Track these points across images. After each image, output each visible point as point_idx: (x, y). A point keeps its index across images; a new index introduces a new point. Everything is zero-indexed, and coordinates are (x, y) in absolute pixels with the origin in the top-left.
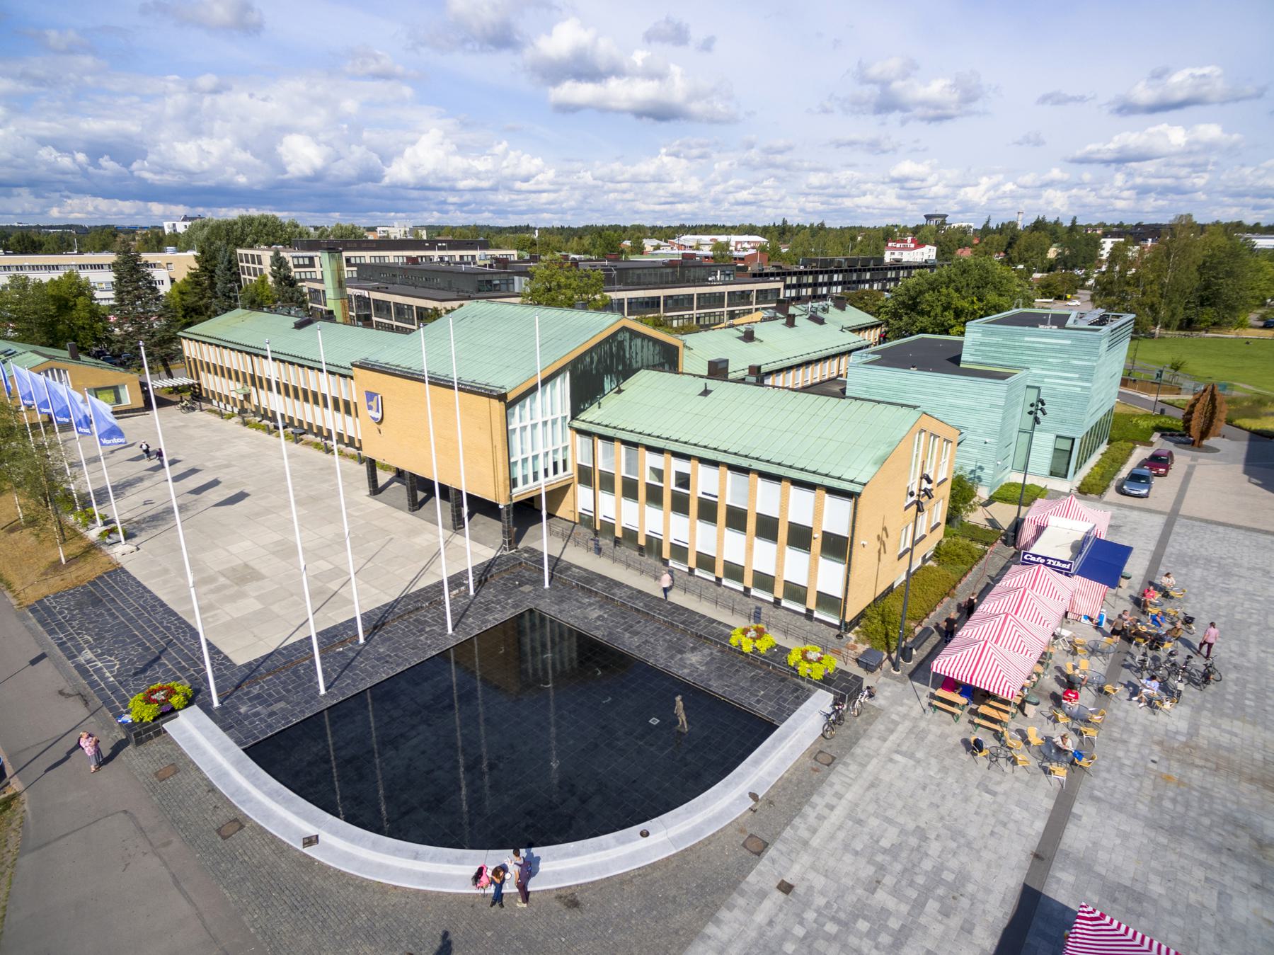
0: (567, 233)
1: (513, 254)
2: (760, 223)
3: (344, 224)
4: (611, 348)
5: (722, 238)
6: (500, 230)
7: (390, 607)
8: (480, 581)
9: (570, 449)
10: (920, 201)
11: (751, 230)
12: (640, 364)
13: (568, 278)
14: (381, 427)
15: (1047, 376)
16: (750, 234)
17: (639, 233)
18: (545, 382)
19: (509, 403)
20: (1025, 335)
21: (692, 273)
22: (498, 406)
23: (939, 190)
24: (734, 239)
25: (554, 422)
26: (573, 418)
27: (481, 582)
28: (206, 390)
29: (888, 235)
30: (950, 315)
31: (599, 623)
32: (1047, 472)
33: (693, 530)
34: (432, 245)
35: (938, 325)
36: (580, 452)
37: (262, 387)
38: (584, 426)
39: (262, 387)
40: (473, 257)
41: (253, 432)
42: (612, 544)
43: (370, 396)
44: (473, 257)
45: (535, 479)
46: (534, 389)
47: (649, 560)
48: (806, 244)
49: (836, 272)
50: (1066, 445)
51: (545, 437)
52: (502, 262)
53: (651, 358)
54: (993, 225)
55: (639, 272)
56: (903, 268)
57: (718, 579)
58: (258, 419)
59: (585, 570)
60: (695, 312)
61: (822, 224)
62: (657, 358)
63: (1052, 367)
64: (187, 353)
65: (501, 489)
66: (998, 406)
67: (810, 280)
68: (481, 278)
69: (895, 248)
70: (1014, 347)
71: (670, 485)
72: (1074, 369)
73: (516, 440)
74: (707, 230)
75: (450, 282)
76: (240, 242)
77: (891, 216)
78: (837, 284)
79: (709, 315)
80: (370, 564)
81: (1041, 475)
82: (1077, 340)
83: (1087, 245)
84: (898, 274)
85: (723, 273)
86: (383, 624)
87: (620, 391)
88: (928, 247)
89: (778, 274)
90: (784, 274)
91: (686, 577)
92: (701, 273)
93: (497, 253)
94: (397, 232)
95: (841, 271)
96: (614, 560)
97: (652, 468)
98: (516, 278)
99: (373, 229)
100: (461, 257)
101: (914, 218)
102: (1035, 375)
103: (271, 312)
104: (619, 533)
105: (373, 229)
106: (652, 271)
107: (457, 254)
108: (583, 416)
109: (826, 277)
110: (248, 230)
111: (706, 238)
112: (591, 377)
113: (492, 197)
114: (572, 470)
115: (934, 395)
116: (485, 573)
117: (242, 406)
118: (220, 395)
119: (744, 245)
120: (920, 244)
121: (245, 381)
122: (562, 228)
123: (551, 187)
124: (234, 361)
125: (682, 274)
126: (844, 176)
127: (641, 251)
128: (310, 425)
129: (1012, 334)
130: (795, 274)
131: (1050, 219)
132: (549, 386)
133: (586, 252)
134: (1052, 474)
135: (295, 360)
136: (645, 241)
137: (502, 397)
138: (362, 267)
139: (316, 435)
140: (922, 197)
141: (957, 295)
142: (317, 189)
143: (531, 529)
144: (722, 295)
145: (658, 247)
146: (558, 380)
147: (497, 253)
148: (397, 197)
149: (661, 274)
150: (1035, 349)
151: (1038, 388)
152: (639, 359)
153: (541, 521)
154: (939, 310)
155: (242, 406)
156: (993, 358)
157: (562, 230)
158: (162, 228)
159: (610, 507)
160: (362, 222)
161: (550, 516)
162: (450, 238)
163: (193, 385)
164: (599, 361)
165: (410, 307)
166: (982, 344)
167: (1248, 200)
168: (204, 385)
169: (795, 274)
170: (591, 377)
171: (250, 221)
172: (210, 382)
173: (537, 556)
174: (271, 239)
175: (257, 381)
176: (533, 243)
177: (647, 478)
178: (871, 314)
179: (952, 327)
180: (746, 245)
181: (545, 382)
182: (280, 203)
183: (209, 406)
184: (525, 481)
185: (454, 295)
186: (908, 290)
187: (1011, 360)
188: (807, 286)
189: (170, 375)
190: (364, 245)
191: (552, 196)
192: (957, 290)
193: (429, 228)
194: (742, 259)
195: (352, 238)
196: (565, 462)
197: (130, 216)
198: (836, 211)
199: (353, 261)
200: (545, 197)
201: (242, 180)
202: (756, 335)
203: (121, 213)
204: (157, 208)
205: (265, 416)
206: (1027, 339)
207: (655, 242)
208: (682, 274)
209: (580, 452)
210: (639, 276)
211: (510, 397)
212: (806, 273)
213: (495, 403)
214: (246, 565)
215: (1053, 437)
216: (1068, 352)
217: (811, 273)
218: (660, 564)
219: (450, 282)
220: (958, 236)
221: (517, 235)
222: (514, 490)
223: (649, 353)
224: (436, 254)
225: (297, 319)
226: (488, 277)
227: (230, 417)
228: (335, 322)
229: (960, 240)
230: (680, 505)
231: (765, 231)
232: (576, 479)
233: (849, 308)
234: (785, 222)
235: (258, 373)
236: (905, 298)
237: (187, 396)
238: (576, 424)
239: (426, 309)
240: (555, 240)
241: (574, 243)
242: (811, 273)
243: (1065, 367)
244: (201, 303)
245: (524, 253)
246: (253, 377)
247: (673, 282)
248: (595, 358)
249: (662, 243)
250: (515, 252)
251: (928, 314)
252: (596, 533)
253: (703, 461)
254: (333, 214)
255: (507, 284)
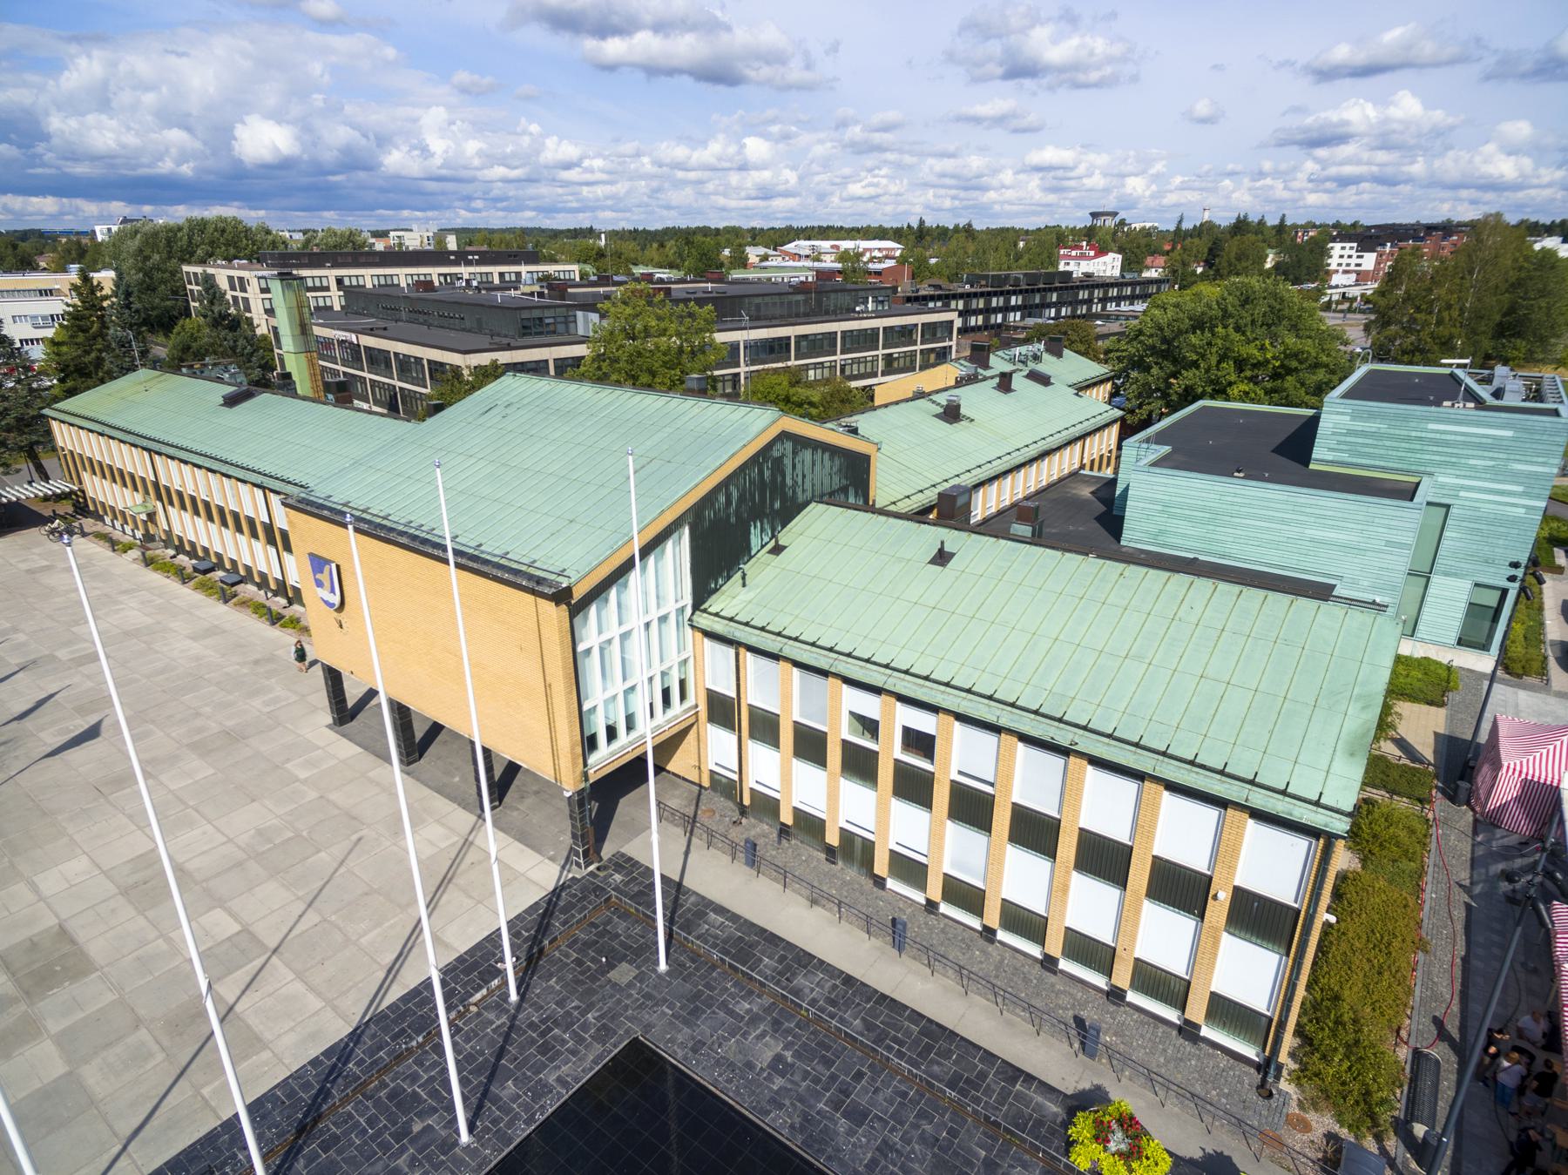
0: (642, 238)
1: (573, 270)
2: (889, 224)
3: (337, 227)
4: (761, 473)
5: (846, 245)
6: (555, 234)
7: (341, 1053)
8: (530, 959)
9: (691, 661)
10: (1073, 195)
11: (881, 233)
12: (809, 494)
13: (659, 318)
14: (343, 616)
15: (1463, 488)
16: (882, 238)
17: (739, 238)
18: (646, 551)
19: (574, 604)
20: (1429, 420)
21: (832, 301)
22: (554, 614)
23: (1096, 181)
24: (864, 244)
25: (663, 619)
26: (698, 605)
27: (530, 965)
28: (94, 501)
29: (1058, 238)
30: (1228, 366)
31: (778, 1082)
32: (1453, 639)
33: (936, 837)
34: (461, 258)
35: (1212, 382)
36: (715, 670)
37: (171, 503)
38: (719, 627)
39: (171, 503)
40: (518, 274)
41: (155, 578)
42: (775, 835)
43: (318, 563)
44: (518, 274)
45: (630, 727)
46: (628, 565)
47: (849, 873)
48: (960, 252)
49: (1014, 293)
50: (1491, 599)
51: (647, 649)
52: (556, 287)
53: (826, 481)
54: (1187, 225)
55: (758, 300)
56: (1098, 286)
57: (988, 933)
58: (171, 552)
59: (735, 918)
60: (838, 357)
61: (970, 225)
62: (836, 479)
63: (1474, 473)
64: (60, 443)
65: (565, 762)
66: (1401, 545)
67: (981, 305)
68: (525, 314)
69: (1070, 257)
70: (1408, 439)
71: (891, 750)
72: (1515, 477)
73: (592, 667)
74: (824, 232)
75: (479, 321)
76: (188, 256)
77: (1038, 214)
78: (1015, 309)
79: (858, 361)
80: (312, 918)
81: (1444, 645)
82: (1525, 430)
83: (1311, 251)
84: (1091, 294)
85: (876, 301)
86: (316, 1121)
87: (778, 550)
88: (1111, 255)
89: (939, 298)
90: (947, 297)
91: (922, 917)
92: (845, 299)
93: (551, 269)
94: (413, 241)
95: (1021, 292)
96: (785, 876)
97: (851, 713)
98: (580, 314)
99: (383, 234)
100: (501, 275)
101: (1081, 220)
102: (1443, 486)
103: (193, 375)
104: (787, 817)
105: (383, 234)
106: (777, 299)
107: (495, 270)
108: (715, 604)
109: (1001, 299)
110: (197, 239)
111: (825, 245)
112: (725, 532)
113: (532, 190)
114: (697, 698)
115: (1283, 521)
116: (538, 929)
117: (147, 530)
118: (112, 509)
119: (880, 253)
120: (1101, 251)
121: (147, 492)
122: (636, 231)
123: (604, 177)
124: (132, 461)
125: (819, 303)
126: (975, 162)
127: (742, 263)
128: (248, 569)
129: (1406, 418)
130: (961, 296)
131: (1254, 218)
132: (651, 559)
133: (671, 266)
134: (1460, 642)
135: (215, 466)
136: (748, 249)
137: (561, 596)
138: (353, 294)
139: (259, 586)
140: (1074, 190)
141: (1237, 337)
142: (273, 179)
143: (623, 801)
144: (875, 331)
145: (765, 258)
146: (669, 544)
147: (551, 269)
148: (406, 193)
149: (790, 303)
150: (1447, 444)
151: (1448, 507)
152: (808, 485)
153: (647, 780)
154: (1214, 360)
155: (147, 530)
156: (1369, 456)
157: (634, 234)
158: (94, 232)
159: (767, 768)
160: (363, 224)
161: (659, 769)
162: (485, 248)
163: (72, 492)
164: (741, 499)
165: (418, 360)
166: (1350, 433)
167: (1464, 193)
168: (90, 493)
169: (961, 296)
170: (725, 532)
171: (202, 225)
172: (98, 489)
173: (636, 872)
174: (232, 251)
175: (161, 492)
176: (601, 254)
177: (845, 731)
178: (1099, 361)
179: (1230, 384)
180: (877, 254)
181: (646, 551)
182: (251, 198)
183: (99, 527)
184: (612, 733)
185: (485, 341)
186: (1161, 329)
187: (1401, 459)
188: (976, 312)
189: (46, 478)
190: (363, 260)
191: (608, 189)
192: (1238, 329)
193: (458, 232)
194: (878, 273)
195: (349, 249)
196: (682, 683)
197: (53, 217)
198: (974, 207)
199: (347, 282)
200: (600, 191)
201: (186, 170)
202: (963, 411)
203: (40, 213)
204: (90, 208)
205: (180, 549)
206: (1431, 426)
207: (762, 250)
208: (819, 303)
209: (715, 670)
210: (758, 306)
211: (578, 594)
212: (975, 295)
213: (548, 607)
214: (63, 933)
215: (1467, 585)
216: (1506, 449)
217: (982, 294)
218: (868, 884)
219: (479, 321)
220: (1143, 241)
221: (578, 241)
222: (593, 759)
223: (823, 473)
224: (464, 271)
225: (232, 389)
226: (536, 314)
227: (127, 548)
228: (295, 395)
229: (1148, 245)
230: (914, 787)
231: (897, 234)
232: (703, 715)
233: (1066, 352)
234: (922, 222)
235: (163, 481)
236: (1156, 341)
237: (66, 508)
238: (703, 621)
239: (442, 364)
240: (629, 247)
241: (653, 251)
242: (982, 294)
243: (1498, 474)
244: (87, 359)
245: (588, 268)
246: (156, 485)
247: (806, 315)
248: (735, 494)
249: (771, 252)
250: (575, 267)
251: (1195, 364)
252: (743, 811)
253: (960, 717)
254: (327, 214)
255: (566, 323)
